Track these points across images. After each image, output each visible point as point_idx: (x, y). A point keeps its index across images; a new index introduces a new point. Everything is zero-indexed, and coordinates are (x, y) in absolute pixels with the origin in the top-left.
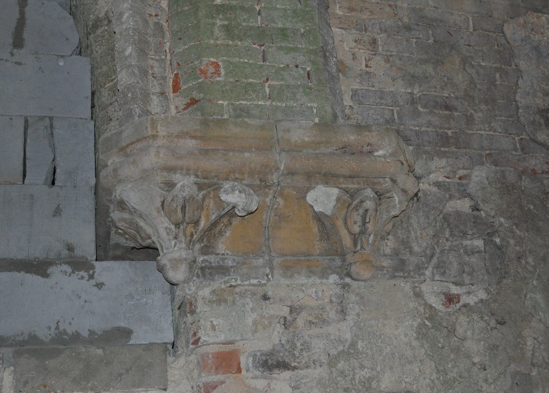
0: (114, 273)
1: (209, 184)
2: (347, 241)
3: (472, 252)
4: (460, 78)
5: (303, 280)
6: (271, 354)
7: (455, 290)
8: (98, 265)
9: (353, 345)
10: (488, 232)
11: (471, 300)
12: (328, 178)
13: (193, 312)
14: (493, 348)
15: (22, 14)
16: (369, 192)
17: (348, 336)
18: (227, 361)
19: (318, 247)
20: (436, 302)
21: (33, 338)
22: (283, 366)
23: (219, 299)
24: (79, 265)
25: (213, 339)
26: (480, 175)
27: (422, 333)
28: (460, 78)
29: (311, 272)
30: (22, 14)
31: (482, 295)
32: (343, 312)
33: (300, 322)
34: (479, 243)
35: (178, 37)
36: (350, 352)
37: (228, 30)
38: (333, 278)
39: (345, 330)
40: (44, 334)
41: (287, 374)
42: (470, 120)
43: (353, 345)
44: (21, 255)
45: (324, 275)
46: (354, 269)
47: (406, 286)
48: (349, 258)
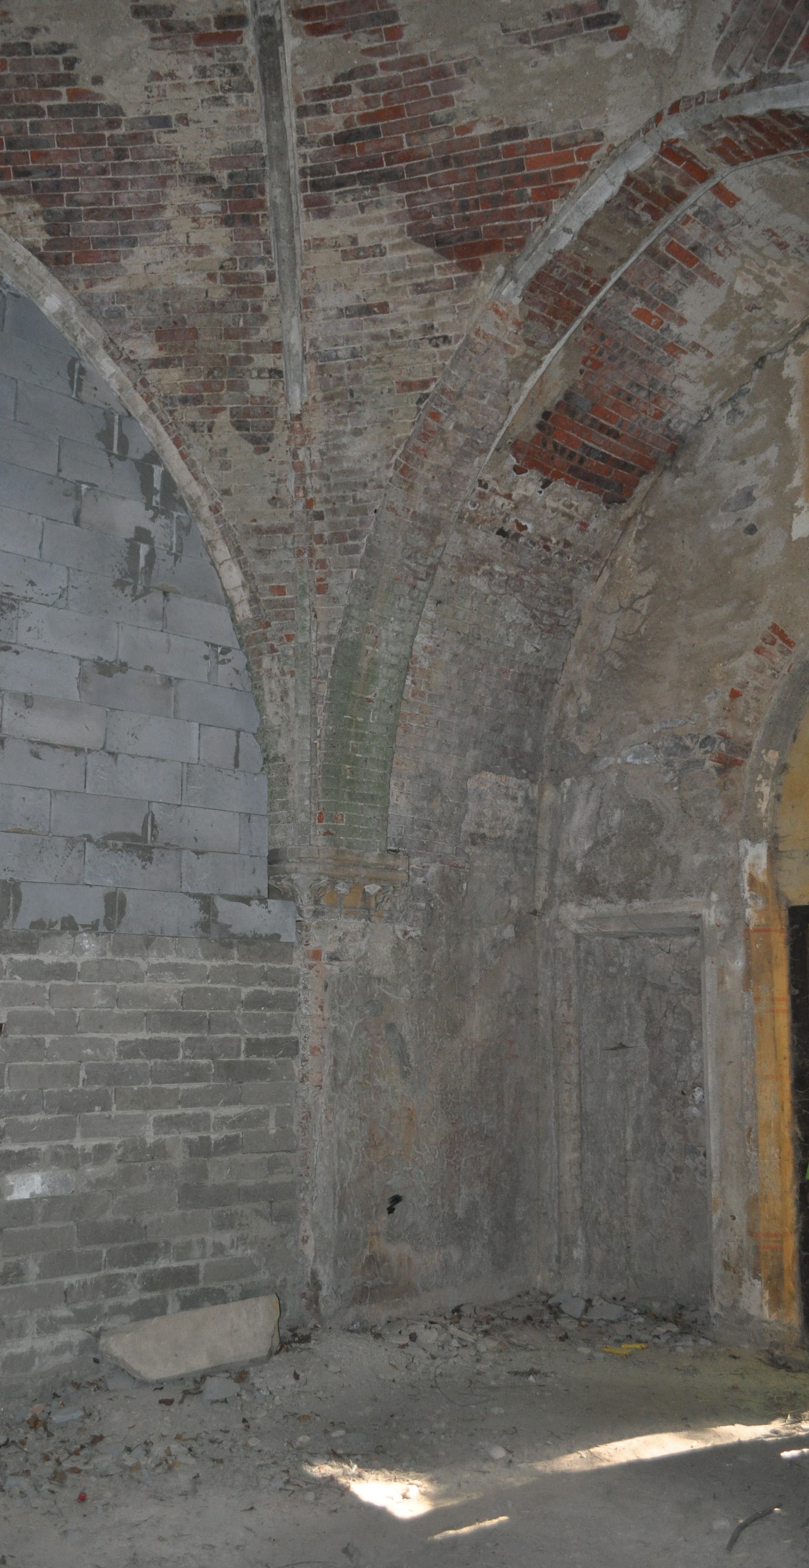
0: (275, 905)
1: (333, 881)
2: (373, 905)
3: (420, 910)
4: (438, 811)
5: (352, 921)
6: (334, 953)
7: (409, 928)
8: (270, 901)
9: (366, 954)
10: (429, 899)
11: (413, 934)
12: (377, 880)
13: (307, 930)
14: (419, 961)
15: (238, 742)
16: (391, 888)
17: (364, 948)
18: (317, 955)
19: (360, 904)
20: (400, 934)
21: (245, 936)
22: (337, 959)
23: (319, 927)
24: (262, 901)
25: (314, 945)
26: (433, 869)
27: (394, 951)
28: (438, 811)
29: (355, 917)
30: (238, 742)
31: (419, 932)
32: (363, 936)
33: (347, 940)
34: (423, 905)
35: (326, 792)
36: (364, 957)
37: (350, 795)
38: (363, 920)
39: (363, 945)
40: (250, 935)
41: (337, 963)
42: (436, 835)
43: (366, 954)
44: (239, 893)
45: (360, 919)
46: (373, 918)
47: (390, 927)
48: (372, 912)
